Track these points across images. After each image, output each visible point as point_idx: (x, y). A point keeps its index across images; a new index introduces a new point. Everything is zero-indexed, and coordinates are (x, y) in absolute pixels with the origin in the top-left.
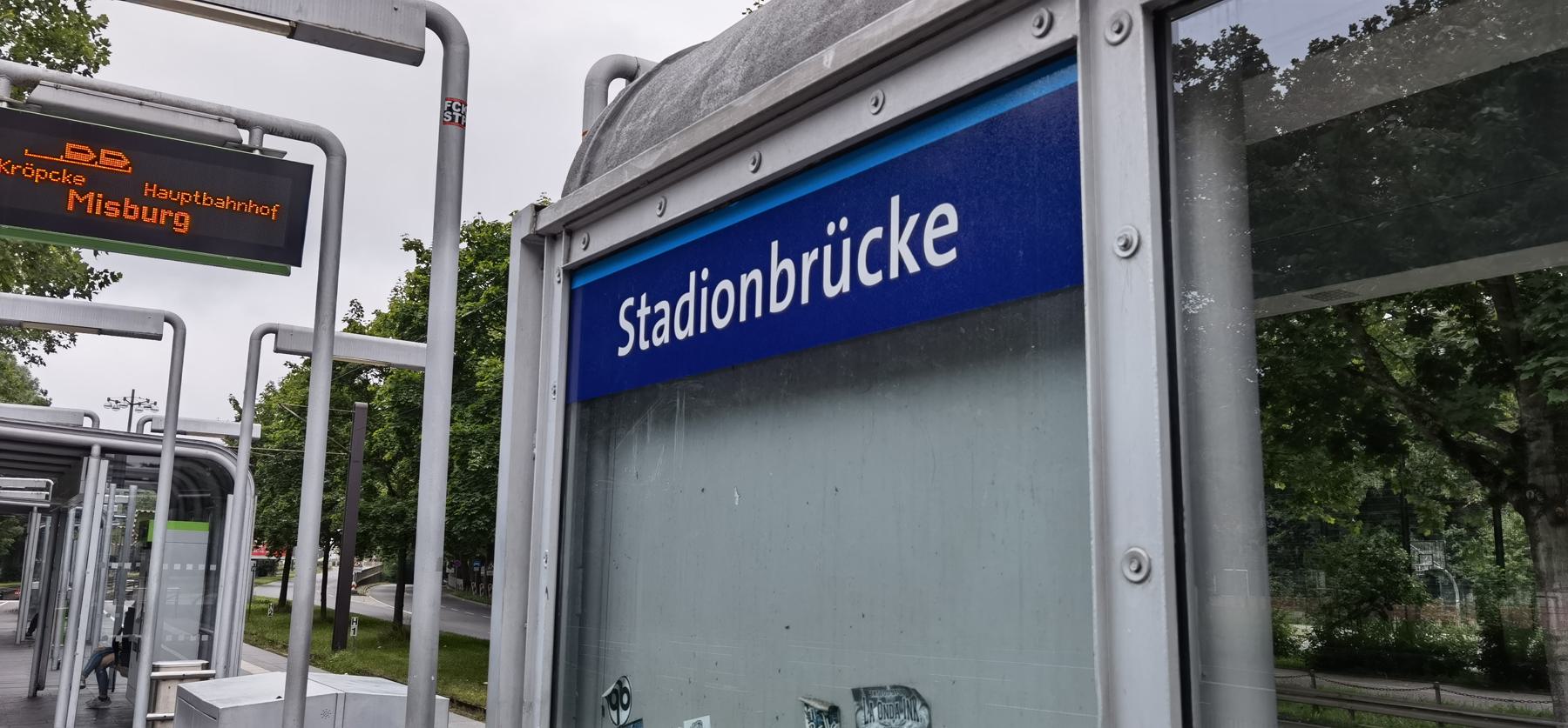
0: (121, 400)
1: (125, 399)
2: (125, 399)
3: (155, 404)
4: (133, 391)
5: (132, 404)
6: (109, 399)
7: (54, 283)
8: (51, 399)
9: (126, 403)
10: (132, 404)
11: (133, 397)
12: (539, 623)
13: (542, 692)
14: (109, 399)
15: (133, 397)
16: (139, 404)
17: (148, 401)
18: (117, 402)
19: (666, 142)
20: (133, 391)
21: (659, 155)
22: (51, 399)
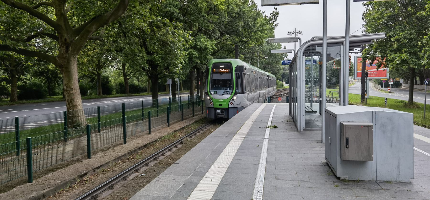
0: (292, 32)
1: (293, 31)
2: (293, 31)
3: (302, 32)
4: (295, 29)
5: (295, 33)
6: (289, 32)
7: (6, 62)
8: (278, 12)
9: (294, 33)
10: (295, 33)
11: (295, 31)
12: (263, 108)
13: (231, 135)
14: (289, 32)
15: (295, 31)
16: (297, 33)
17: (300, 31)
18: (291, 33)
19: (111, 128)
20: (295, 29)
21: (337, 126)
22: (278, 12)
